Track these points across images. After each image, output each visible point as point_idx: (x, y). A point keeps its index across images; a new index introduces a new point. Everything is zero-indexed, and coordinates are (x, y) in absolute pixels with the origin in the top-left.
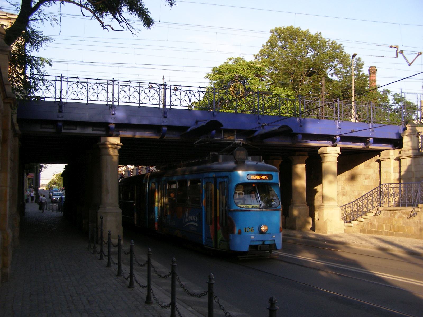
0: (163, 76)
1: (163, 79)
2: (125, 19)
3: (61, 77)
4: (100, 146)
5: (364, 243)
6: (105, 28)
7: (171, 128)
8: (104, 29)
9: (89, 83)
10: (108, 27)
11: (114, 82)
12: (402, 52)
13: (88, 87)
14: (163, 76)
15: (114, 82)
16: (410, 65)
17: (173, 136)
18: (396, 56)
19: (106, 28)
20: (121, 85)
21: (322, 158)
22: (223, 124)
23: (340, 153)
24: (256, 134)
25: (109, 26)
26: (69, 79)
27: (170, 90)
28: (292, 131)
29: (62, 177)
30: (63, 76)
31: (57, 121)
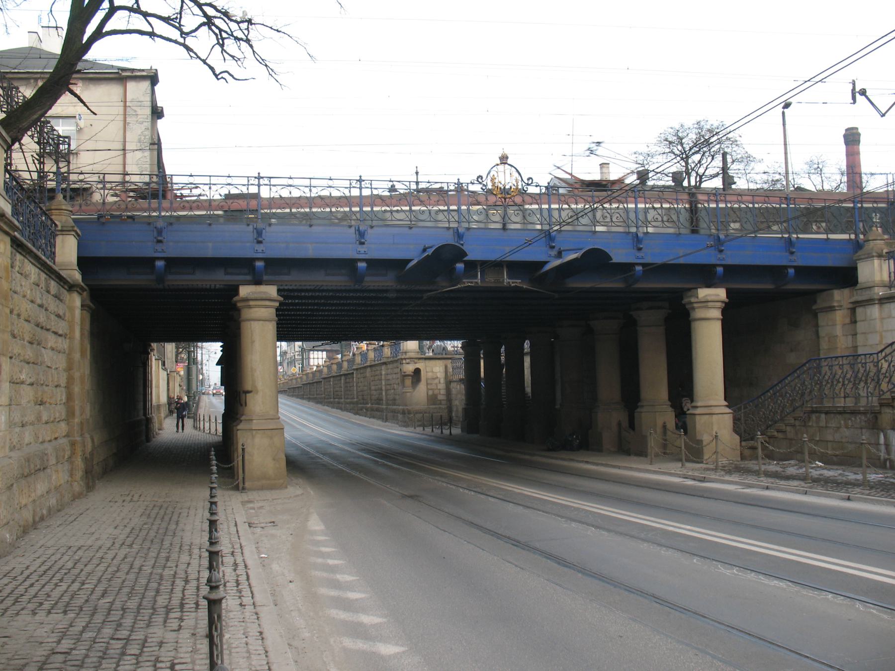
0: (417, 167)
1: (417, 173)
2: (263, 60)
3: (259, 178)
4: (239, 305)
5: (634, 466)
6: (219, 77)
7: (373, 263)
8: (218, 79)
9: (213, 184)
10: (225, 75)
11: (261, 180)
12: (863, 92)
13: (212, 192)
14: (417, 167)
15: (363, 183)
16: (883, 115)
17: (386, 281)
18: (852, 101)
19: (222, 78)
20: (274, 185)
21: (691, 311)
22: (612, 257)
23: (727, 300)
24: (548, 267)
25: (226, 74)
26: (273, 181)
27: (247, 183)
28: (611, 259)
29: (219, 367)
30: (261, 175)
31: (152, 260)
